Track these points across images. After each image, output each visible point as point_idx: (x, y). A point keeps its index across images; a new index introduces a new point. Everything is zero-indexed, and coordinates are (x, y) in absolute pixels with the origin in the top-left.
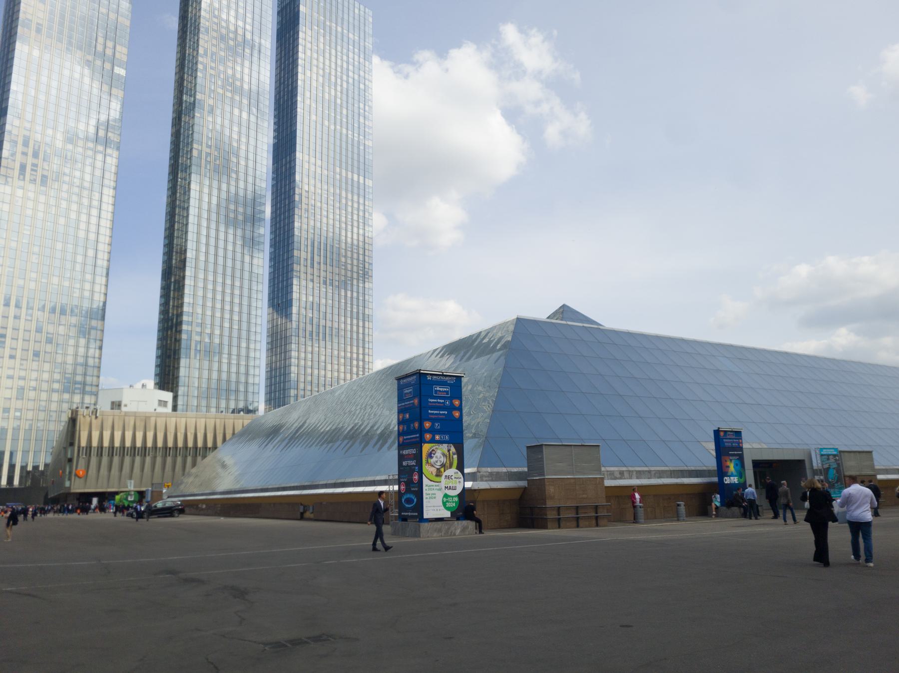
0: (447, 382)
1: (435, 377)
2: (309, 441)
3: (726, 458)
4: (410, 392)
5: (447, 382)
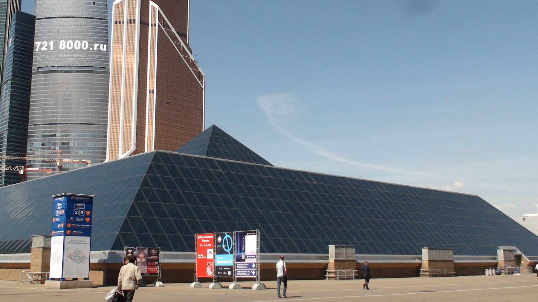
0: (83, 200)
1: (76, 198)
2: (11, 196)
3: (66, 197)
4: (61, 206)
5: (83, 200)
